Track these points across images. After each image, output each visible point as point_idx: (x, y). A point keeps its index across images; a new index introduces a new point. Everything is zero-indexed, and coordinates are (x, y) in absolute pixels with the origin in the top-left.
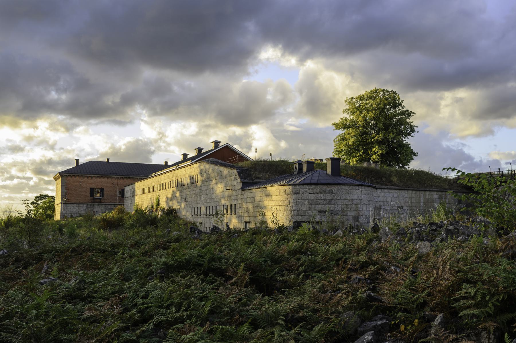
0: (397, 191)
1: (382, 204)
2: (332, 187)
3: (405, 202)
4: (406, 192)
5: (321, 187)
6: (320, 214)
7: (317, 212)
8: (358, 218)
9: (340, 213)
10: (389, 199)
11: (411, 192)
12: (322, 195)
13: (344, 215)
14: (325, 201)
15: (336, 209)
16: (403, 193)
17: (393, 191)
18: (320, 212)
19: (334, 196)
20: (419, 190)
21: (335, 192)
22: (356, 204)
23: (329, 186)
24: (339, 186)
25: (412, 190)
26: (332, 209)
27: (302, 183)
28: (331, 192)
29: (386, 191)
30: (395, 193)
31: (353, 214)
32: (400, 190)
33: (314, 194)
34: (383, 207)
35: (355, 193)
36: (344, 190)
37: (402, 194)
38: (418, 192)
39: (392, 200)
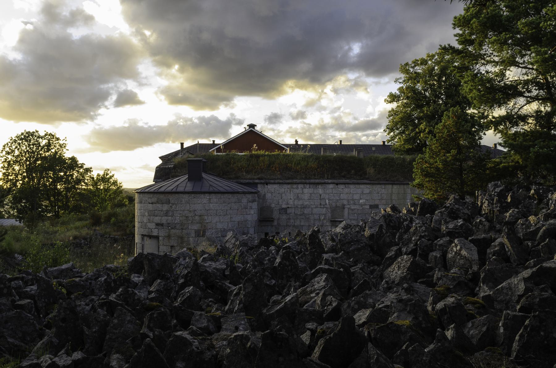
0: (368, 186)
1: (345, 202)
2: (169, 196)
3: (382, 199)
4: (384, 187)
5: (158, 196)
6: (157, 227)
7: (155, 224)
8: (204, 232)
9: (178, 227)
10: (356, 197)
11: (390, 186)
12: (159, 206)
13: (183, 229)
14: (162, 213)
15: (173, 221)
16: (377, 188)
17: (362, 186)
18: (157, 224)
19: (171, 207)
20: (404, 184)
21: (172, 201)
22: (200, 216)
23: (167, 195)
24: (177, 195)
25: (392, 184)
26: (169, 222)
27: (156, 191)
28: (168, 202)
29: (352, 186)
30: (366, 189)
31: (196, 227)
32: (373, 184)
33: (152, 203)
34: (348, 206)
35: (199, 202)
36: (183, 200)
37: (376, 189)
38: (402, 186)
39: (361, 197)
